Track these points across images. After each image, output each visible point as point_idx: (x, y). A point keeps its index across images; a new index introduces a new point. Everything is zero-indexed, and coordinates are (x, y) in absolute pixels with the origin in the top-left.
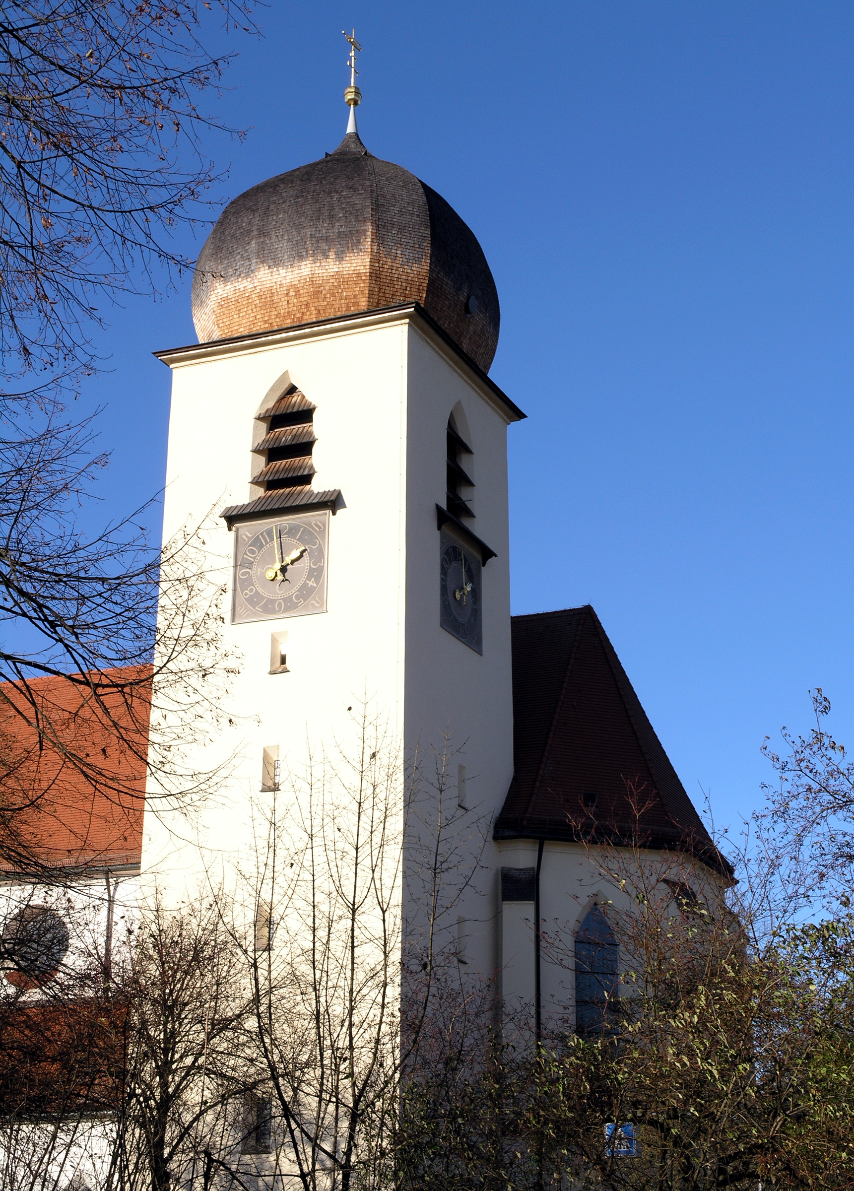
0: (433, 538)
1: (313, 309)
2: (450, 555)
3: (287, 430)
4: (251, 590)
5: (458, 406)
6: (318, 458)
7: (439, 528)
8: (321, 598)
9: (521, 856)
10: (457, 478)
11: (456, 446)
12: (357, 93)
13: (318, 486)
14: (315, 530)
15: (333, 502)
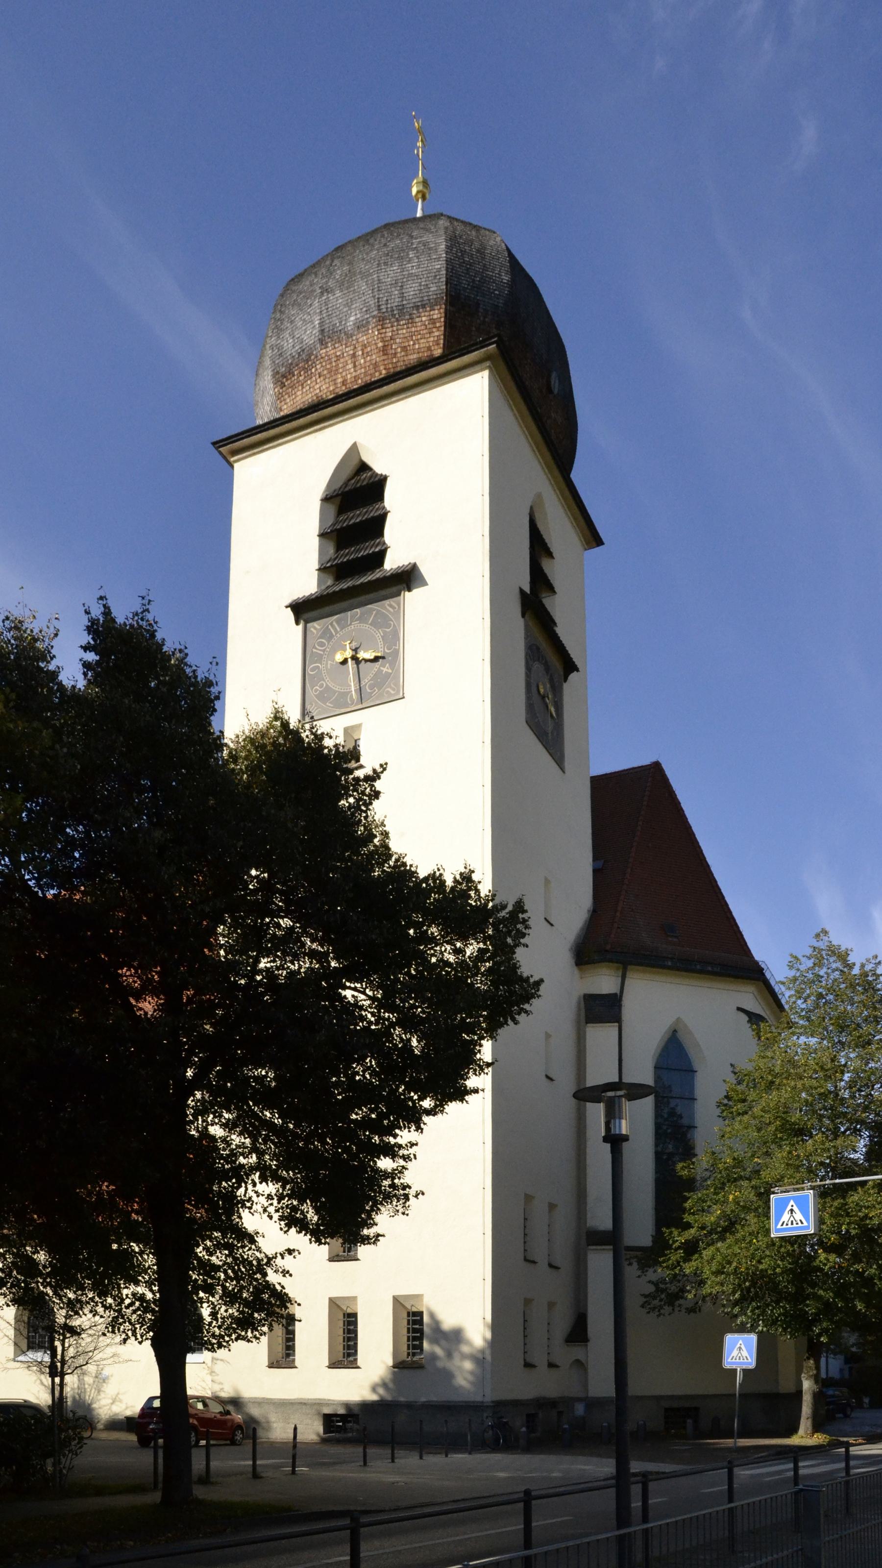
0: (517, 624)
1: (382, 368)
2: (533, 653)
3: (356, 504)
4: (321, 686)
5: (539, 496)
6: (391, 533)
7: (523, 615)
8: (397, 684)
9: (604, 982)
10: (540, 581)
11: (539, 547)
12: (425, 183)
13: (392, 562)
14: (388, 611)
15: (408, 578)
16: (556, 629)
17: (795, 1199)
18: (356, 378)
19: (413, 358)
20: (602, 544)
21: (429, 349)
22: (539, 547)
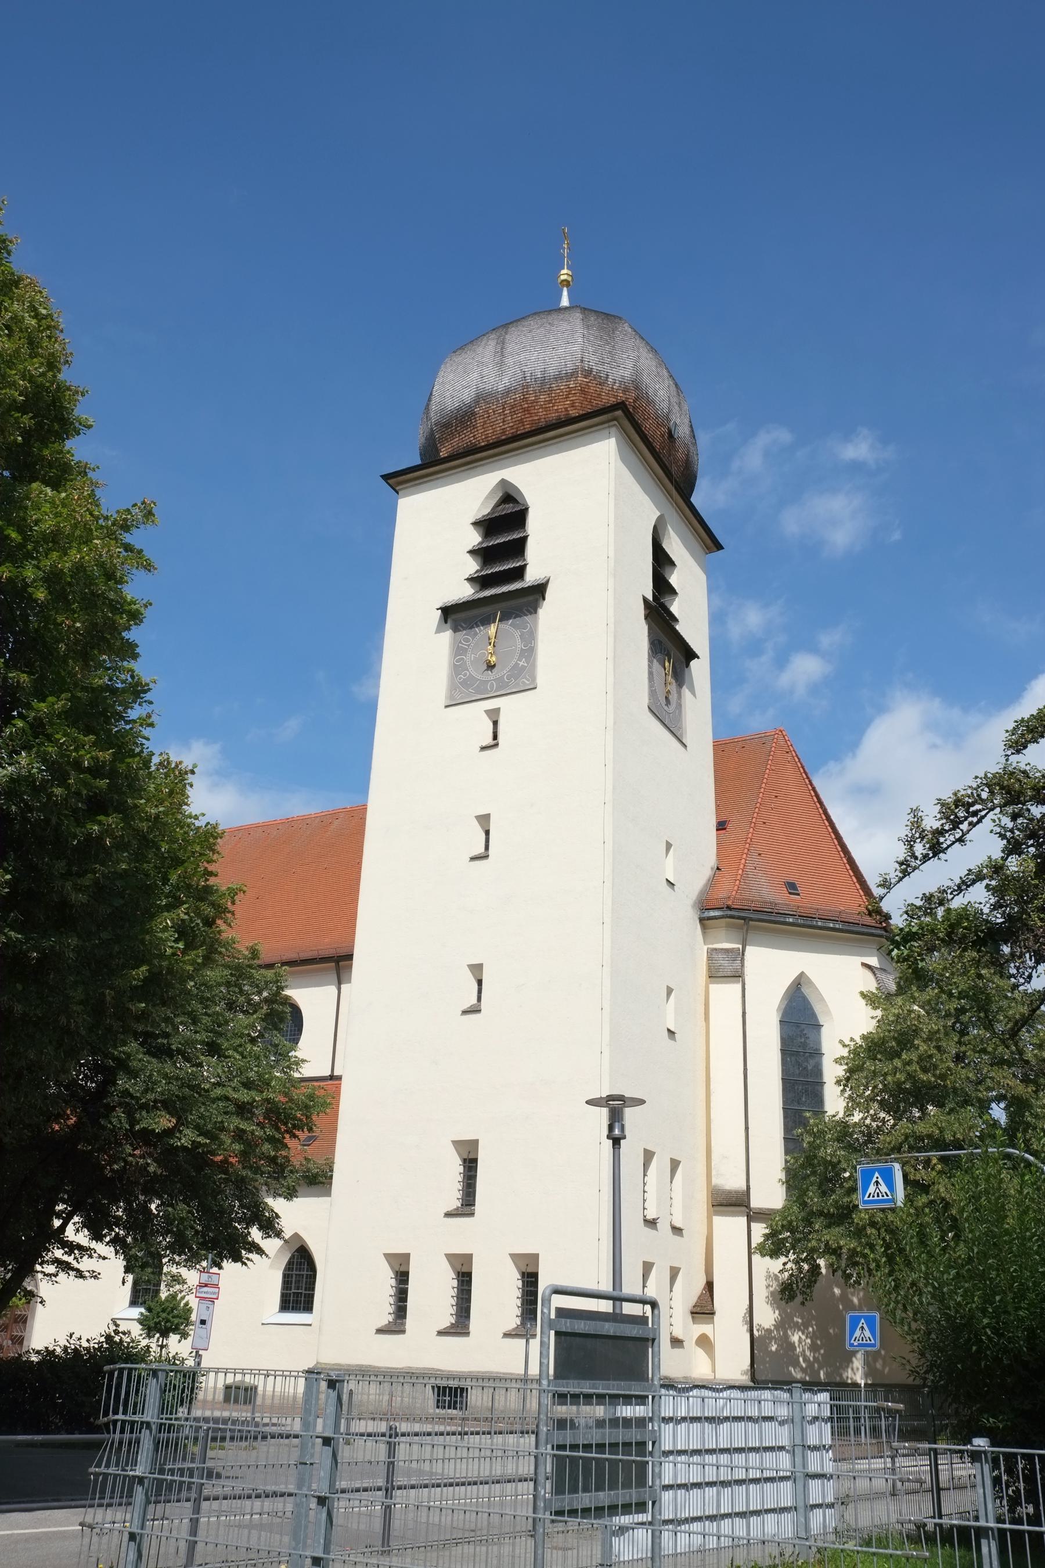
3: (504, 531)
11: (661, 560)
16: (677, 627)
17: (866, 1318)
18: (504, 431)
19: (553, 416)
20: (722, 548)
21: (566, 409)
22: (661, 560)
